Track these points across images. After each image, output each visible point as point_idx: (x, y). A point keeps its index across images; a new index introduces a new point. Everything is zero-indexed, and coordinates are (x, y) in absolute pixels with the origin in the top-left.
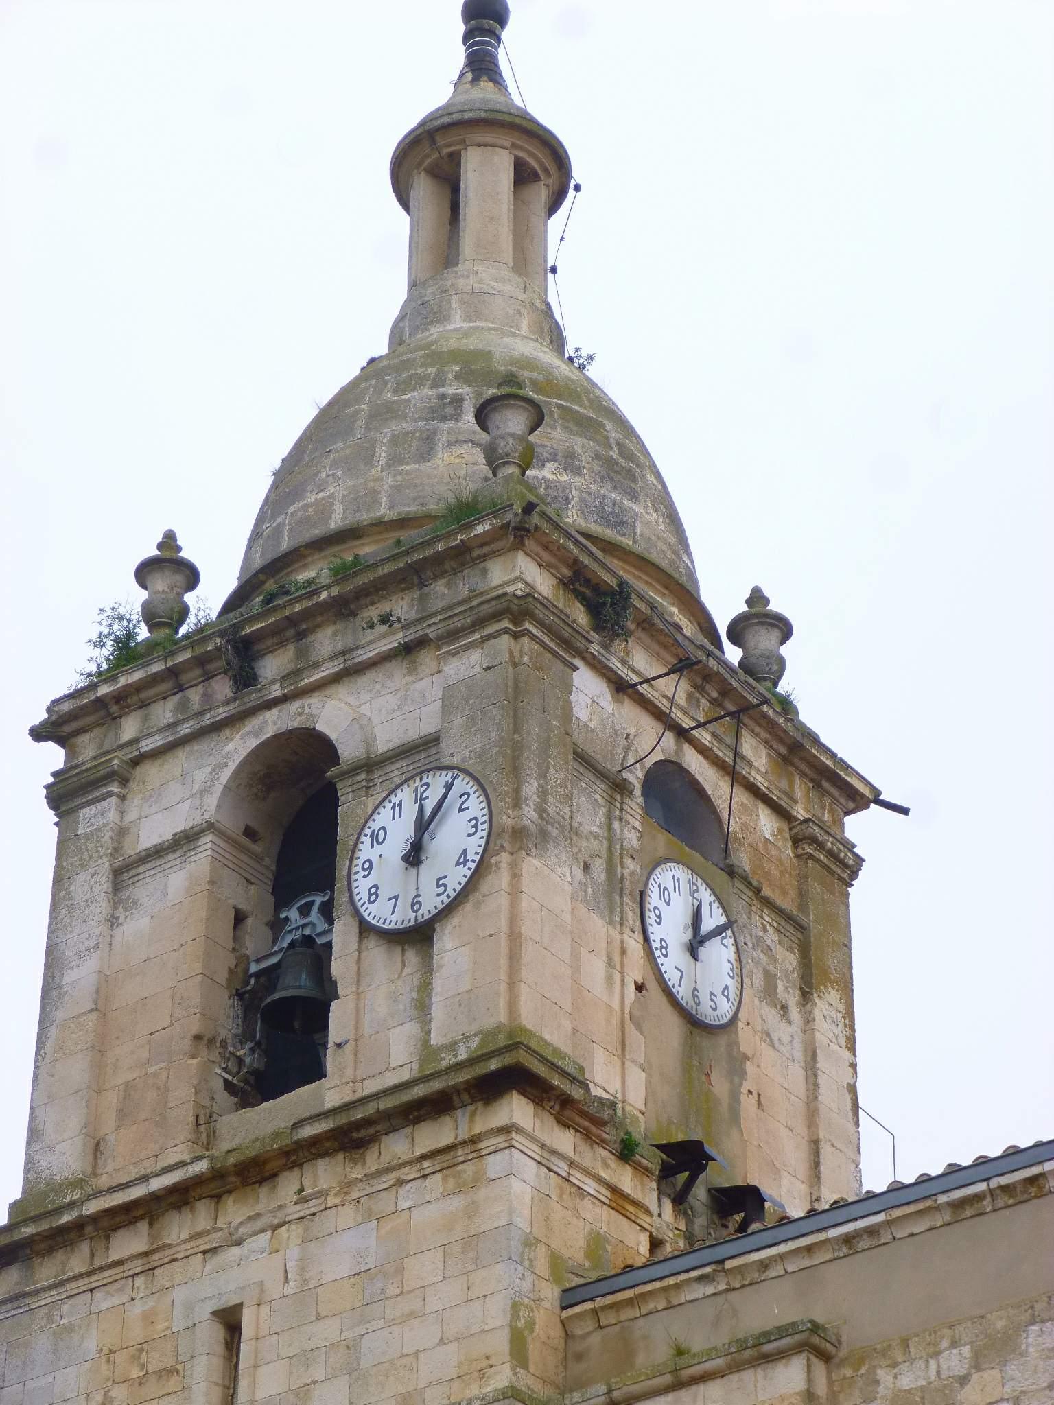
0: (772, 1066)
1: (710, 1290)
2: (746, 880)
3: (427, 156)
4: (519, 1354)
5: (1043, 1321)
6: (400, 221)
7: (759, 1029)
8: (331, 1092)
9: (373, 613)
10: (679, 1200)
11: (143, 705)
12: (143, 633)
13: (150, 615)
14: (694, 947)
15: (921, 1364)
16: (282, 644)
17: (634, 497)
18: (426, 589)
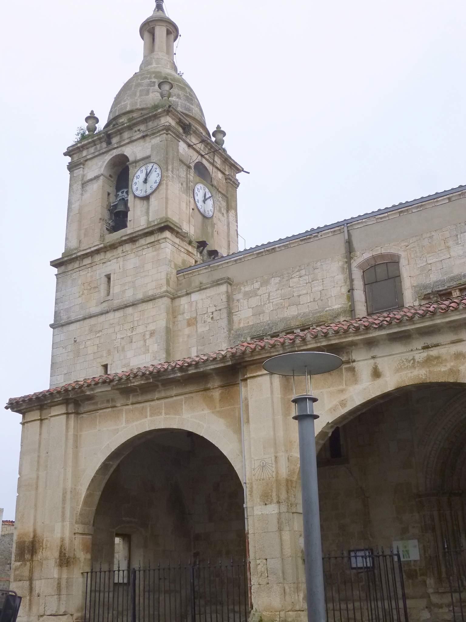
0: (220, 226)
1: (207, 271)
2: (215, 187)
4: (168, 283)
6: (142, 42)
8: (128, 230)
9: (136, 129)
10: (201, 253)
12: (87, 133)
13: (88, 129)
14: (204, 201)
16: (117, 135)
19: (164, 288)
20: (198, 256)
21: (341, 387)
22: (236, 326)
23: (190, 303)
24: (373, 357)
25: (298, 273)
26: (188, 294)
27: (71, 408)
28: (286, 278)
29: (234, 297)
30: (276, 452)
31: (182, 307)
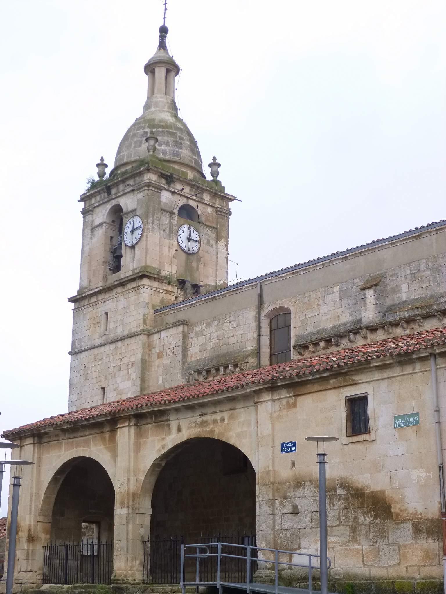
2: (202, 223)
11: (95, 196)
16: (115, 187)
17: (181, 148)
19: (141, 328)
20: (177, 292)
21: (163, 437)
22: (189, 360)
23: (160, 339)
24: (178, 419)
26: (158, 332)
27: (36, 440)
28: (221, 322)
29: (189, 335)
30: (129, 476)
31: (155, 342)
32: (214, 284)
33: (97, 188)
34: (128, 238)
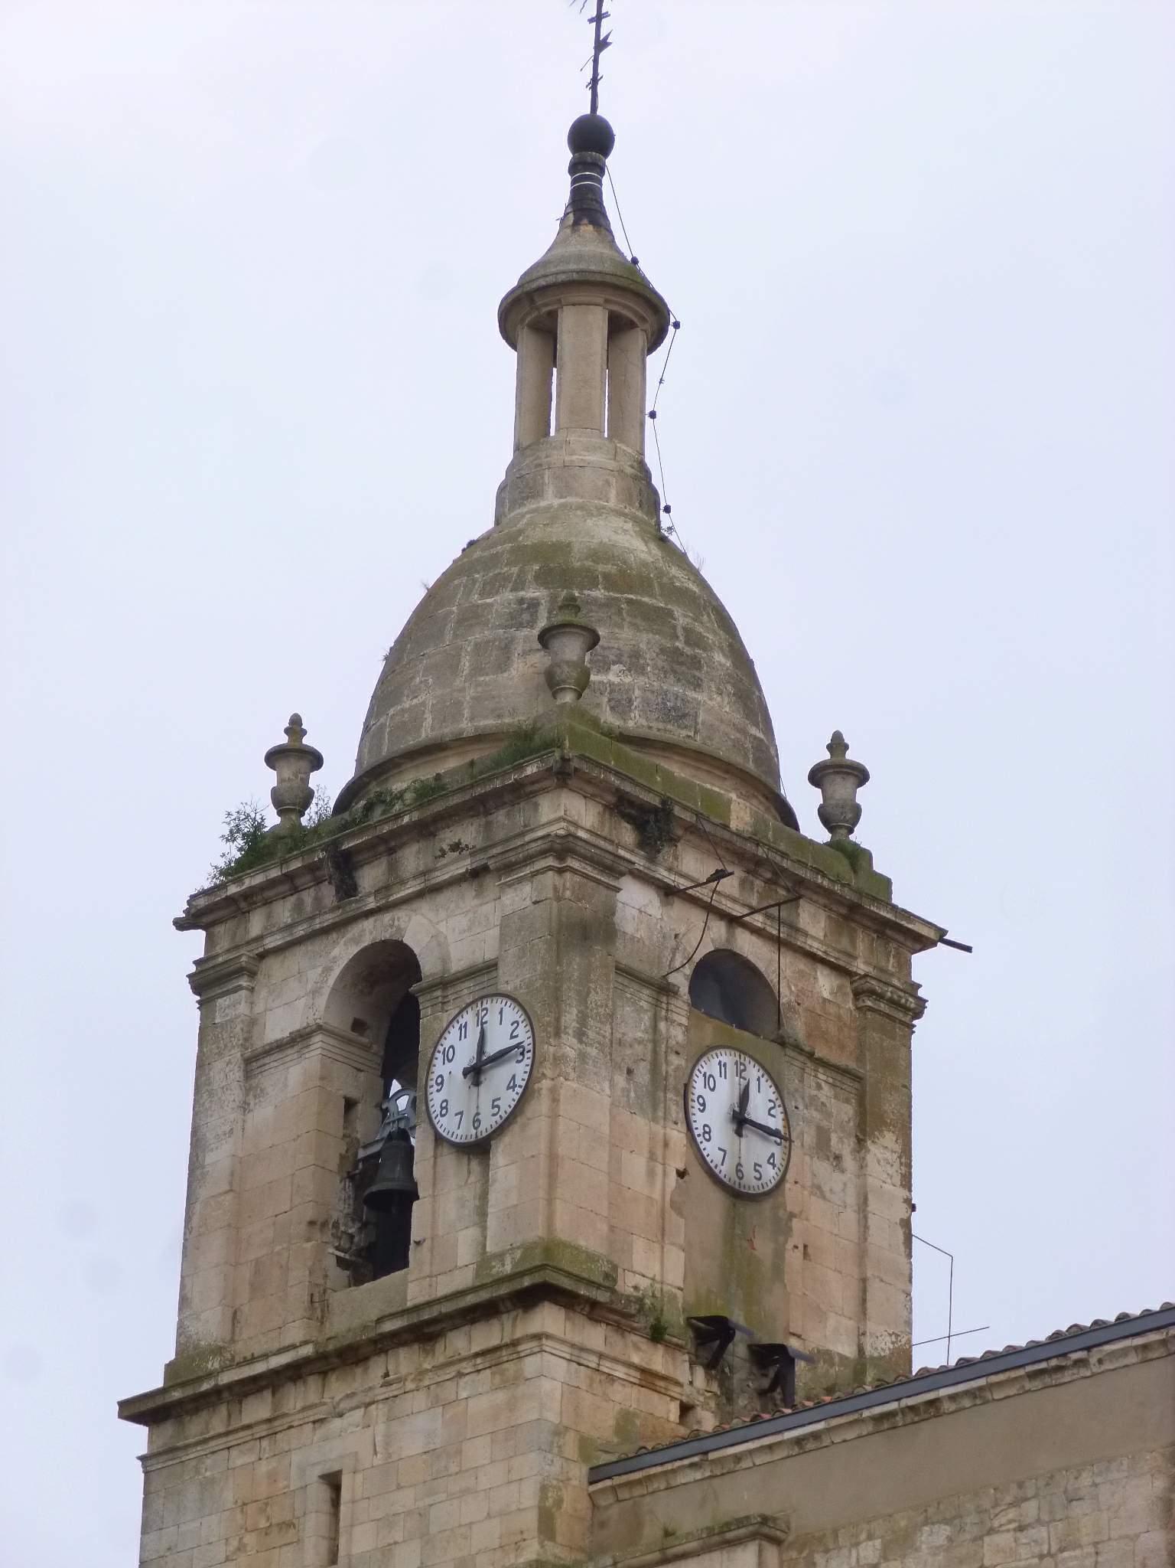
0: (822, 1211)
1: (698, 1475)
2: (798, 1048)
3: (528, 314)
4: (547, 1526)
5: (933, 1524)
7: (809, 1184)
11: (267, 902)
13: (279, 801)
15: (845, 1551)
16: (377, 857)
17: (697, 685)
18: (490, 818)
20: (695, 1381)
25: (1012, 1514)
32: (848, 1350)
33: (285, 862)
34: (451, 1101)
